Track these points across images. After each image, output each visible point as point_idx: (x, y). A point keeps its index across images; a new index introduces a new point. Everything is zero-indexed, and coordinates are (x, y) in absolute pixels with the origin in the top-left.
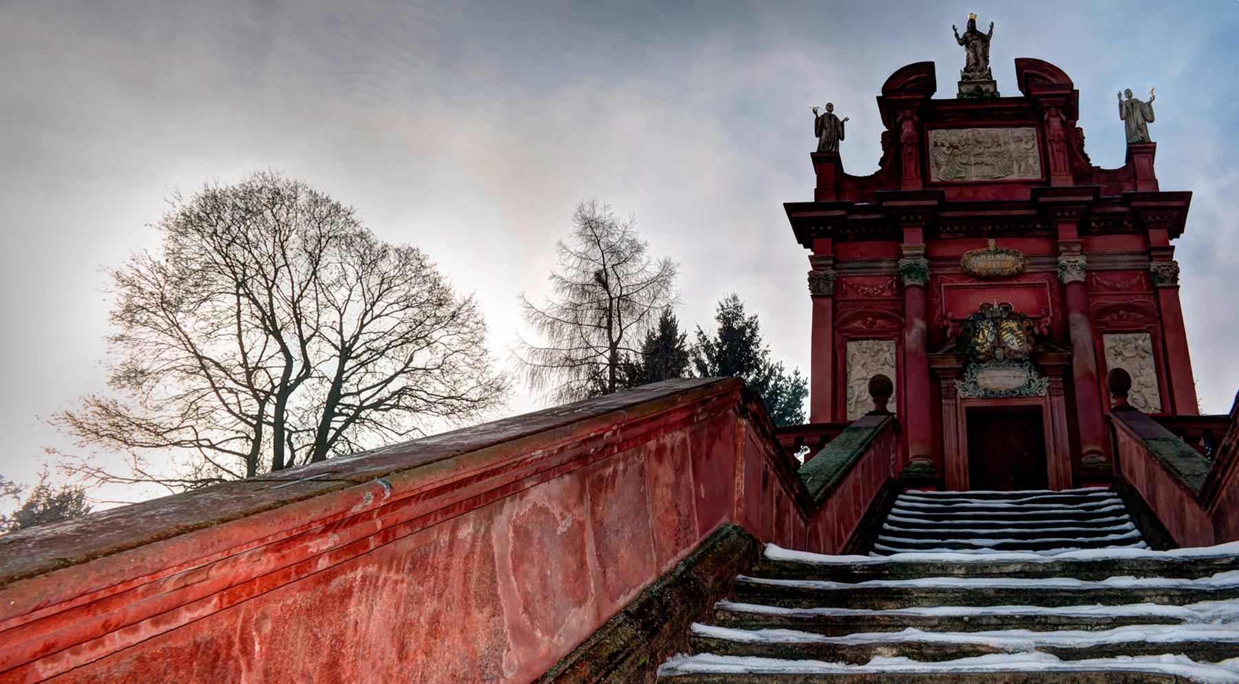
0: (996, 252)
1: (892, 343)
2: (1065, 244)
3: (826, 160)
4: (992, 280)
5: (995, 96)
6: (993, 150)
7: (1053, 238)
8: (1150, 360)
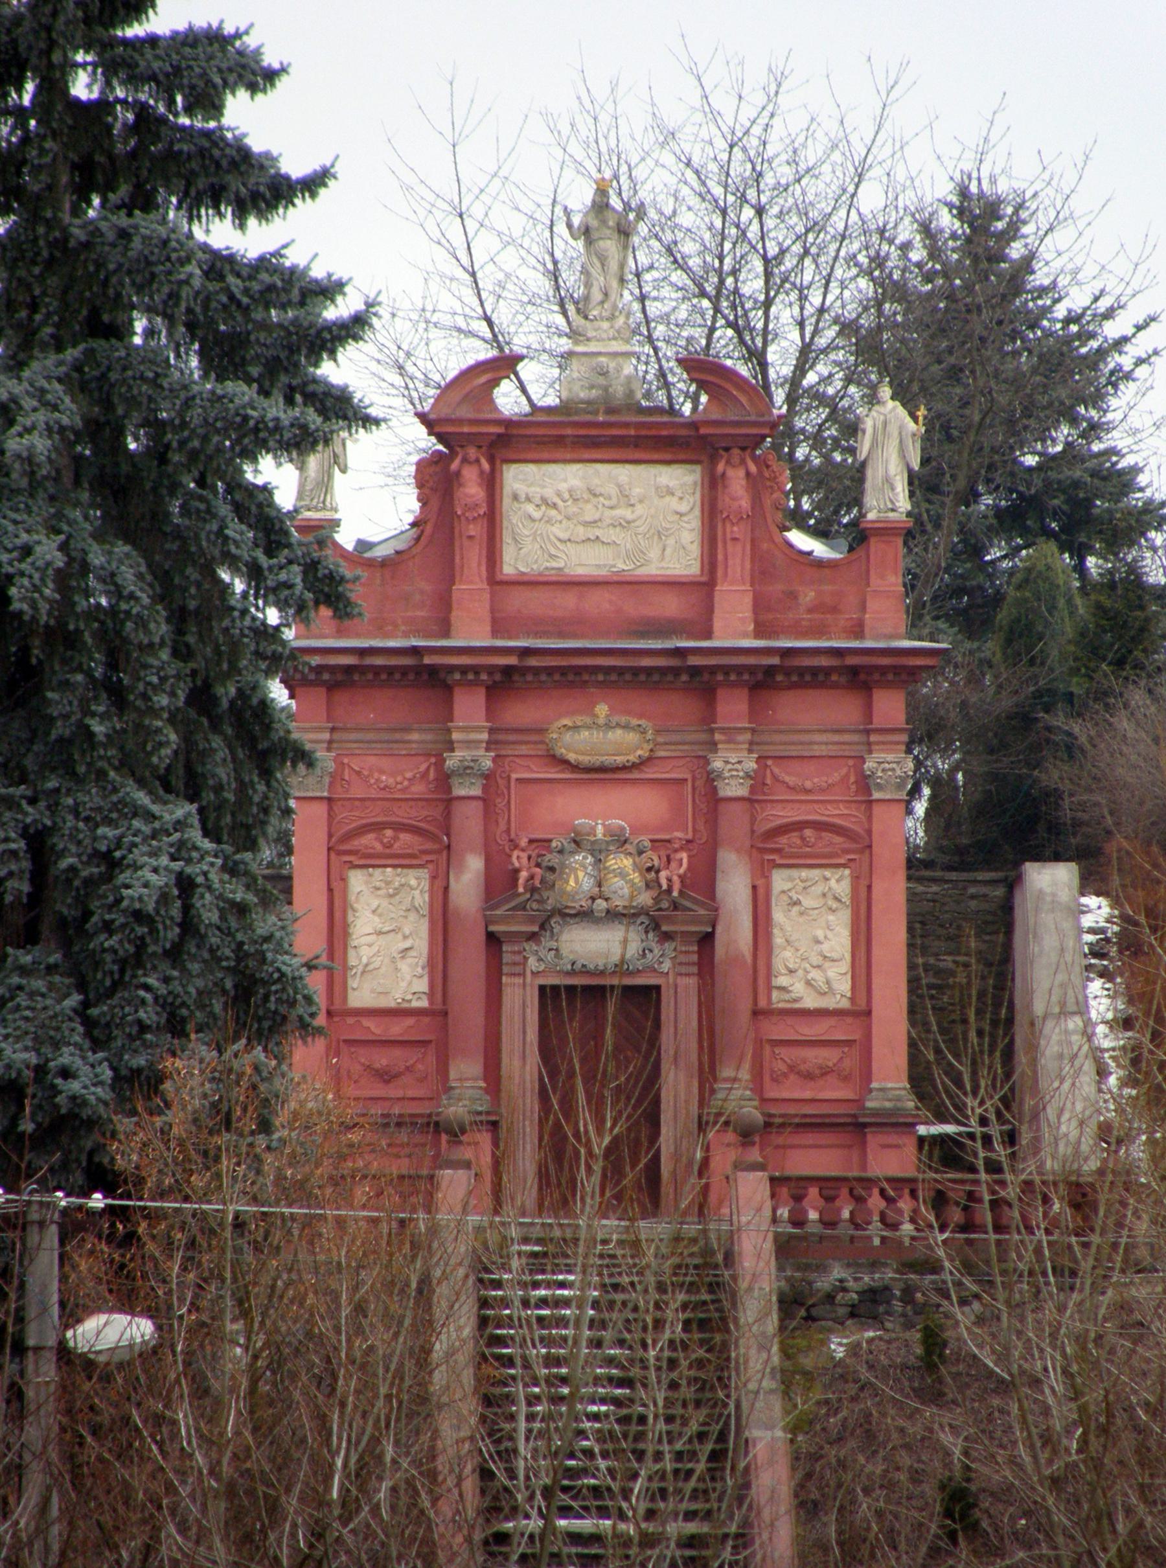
0: (608, 726)
1: (424, 874)
2: (723, 730)
6: (618, 512)
7: (708, 719)
8: (845, 915)
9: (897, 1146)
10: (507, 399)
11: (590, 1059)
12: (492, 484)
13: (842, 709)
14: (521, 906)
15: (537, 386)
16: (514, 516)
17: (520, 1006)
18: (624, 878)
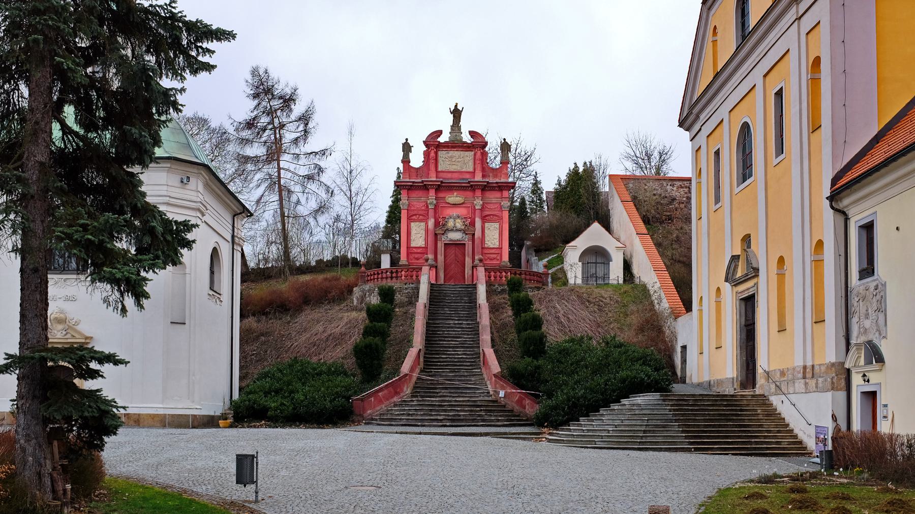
3: (406, 161)
4: (455, 205)
5: (461, 140)
9: (684, 348)
10: (442, 139)
11: (674, 410)
12: (436, 153)
13: (498, 194)
15: (444, 138)
16: (440, 160)
17: (440, 246)
18: (459, 224)
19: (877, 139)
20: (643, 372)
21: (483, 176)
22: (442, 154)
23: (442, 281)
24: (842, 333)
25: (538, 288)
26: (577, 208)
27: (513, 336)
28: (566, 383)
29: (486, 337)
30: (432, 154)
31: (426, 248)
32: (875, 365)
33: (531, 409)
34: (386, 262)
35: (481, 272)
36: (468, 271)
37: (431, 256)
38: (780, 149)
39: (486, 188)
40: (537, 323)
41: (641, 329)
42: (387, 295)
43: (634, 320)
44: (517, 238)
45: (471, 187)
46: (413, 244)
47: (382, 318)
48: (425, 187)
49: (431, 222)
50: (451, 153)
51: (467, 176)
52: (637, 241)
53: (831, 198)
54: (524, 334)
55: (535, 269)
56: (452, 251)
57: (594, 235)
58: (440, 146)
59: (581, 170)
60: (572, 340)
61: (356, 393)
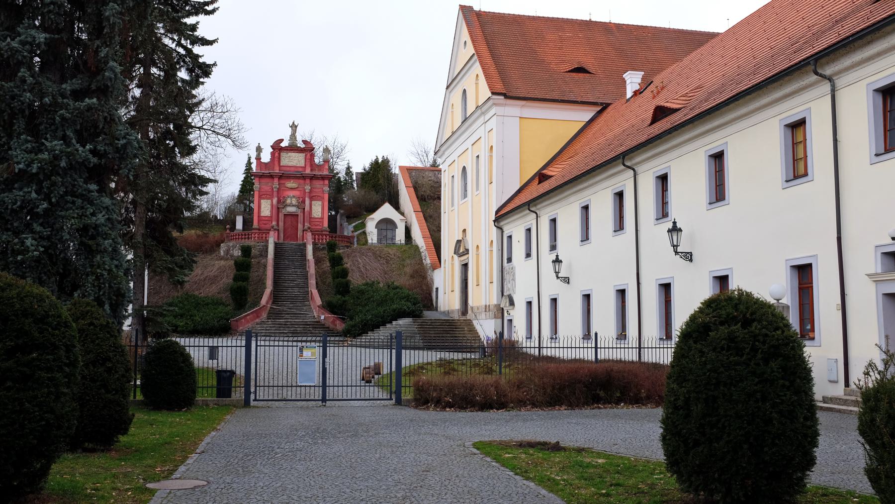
4: (292, 189)
9: (437, 289)
10: (283, 145)
13: (321, 182)
14: (281, 203)
16: (282, 159)
17: (281, 216)
18: (294, 201)
19: (519, 191)
20: (406, 306)
21: (311, 170)
22: (283, 155)
23: (281, 241)
24: (500, 289)
25: (348, 247)
26: (376, 187)
27: (330, 280)
28: (361, 311)
29: (312, 282)
30: (277, 155)
31: (271, 217)
32: (511, 307)
33: (340, 326)
34: (239, 225)
35: (309, 236)
36: (300, 233)
37: (274, 223)
38: (477, 189)
39: (313, 178)
40: (345, 273)
41: (412, 276)
42: (246, 251)
43: (408, 270)
44: (335, 203)
45: (304, 177)
46: (262, 214)
47: (244, 266)
48: (271, 177)
49: (275, 200)
50: (290, 154)
51: (300, 170)
52: (414, 215)
53: (494, 221)
54: (337, 280)
55: (346, 234)
56: (289, 219)
57: (386, 211)
58: (282, 149)
59: (380, 161)
60: (367, 284)
61: (232, 317)
